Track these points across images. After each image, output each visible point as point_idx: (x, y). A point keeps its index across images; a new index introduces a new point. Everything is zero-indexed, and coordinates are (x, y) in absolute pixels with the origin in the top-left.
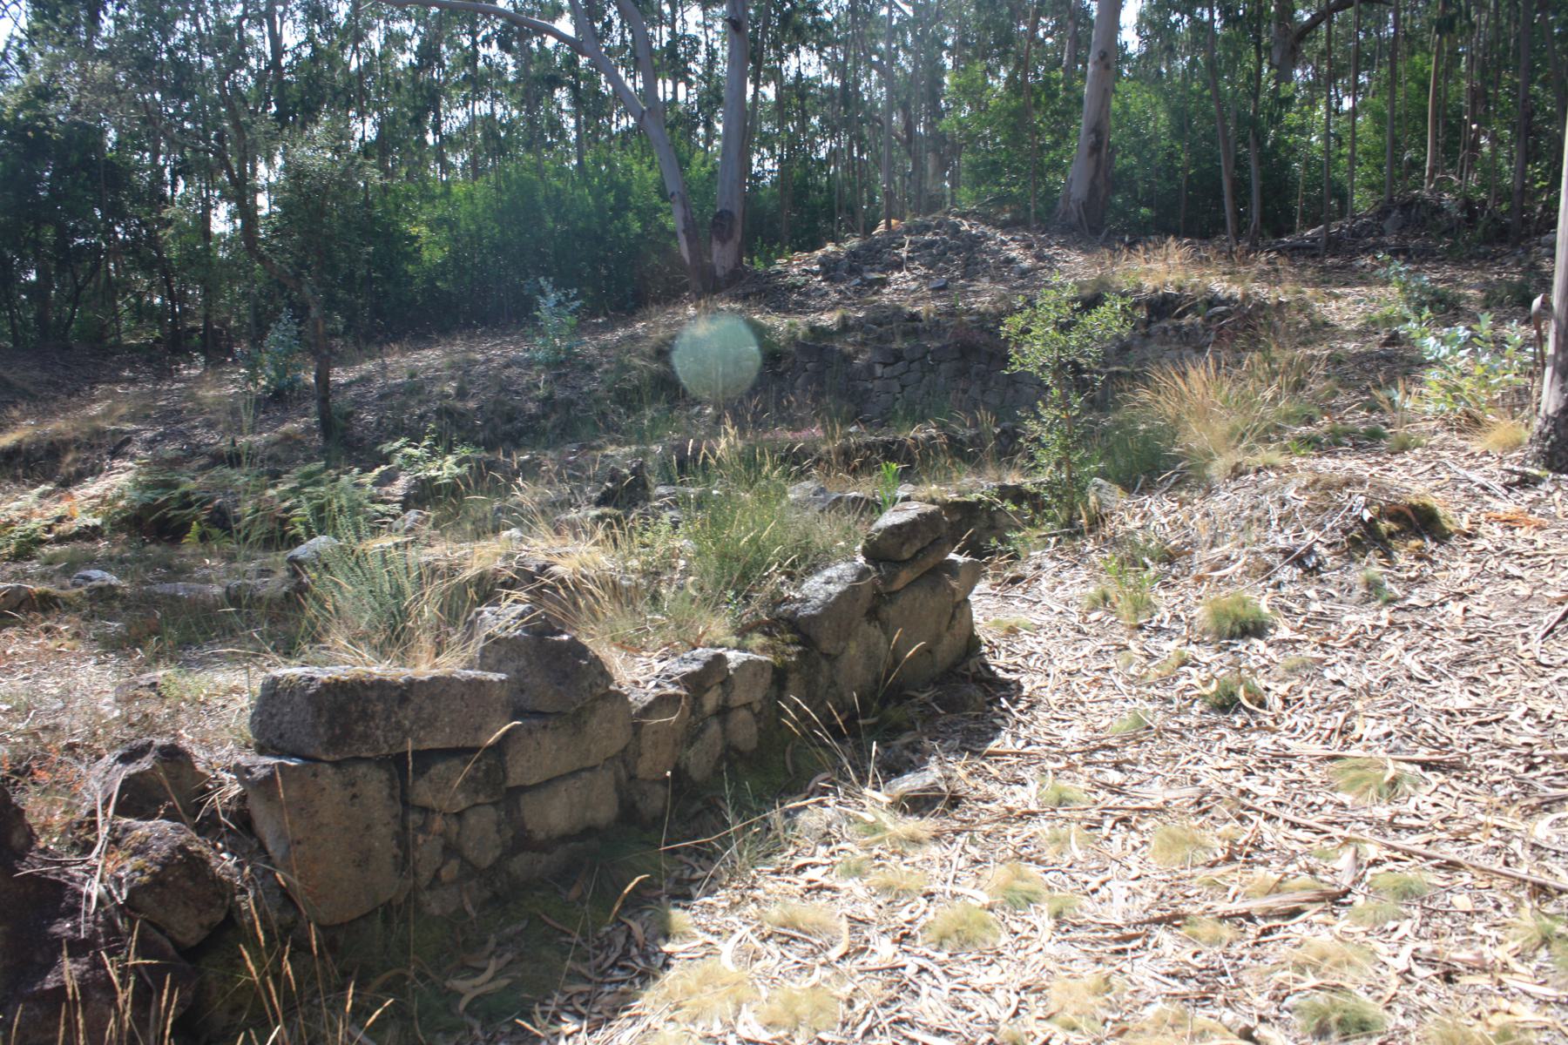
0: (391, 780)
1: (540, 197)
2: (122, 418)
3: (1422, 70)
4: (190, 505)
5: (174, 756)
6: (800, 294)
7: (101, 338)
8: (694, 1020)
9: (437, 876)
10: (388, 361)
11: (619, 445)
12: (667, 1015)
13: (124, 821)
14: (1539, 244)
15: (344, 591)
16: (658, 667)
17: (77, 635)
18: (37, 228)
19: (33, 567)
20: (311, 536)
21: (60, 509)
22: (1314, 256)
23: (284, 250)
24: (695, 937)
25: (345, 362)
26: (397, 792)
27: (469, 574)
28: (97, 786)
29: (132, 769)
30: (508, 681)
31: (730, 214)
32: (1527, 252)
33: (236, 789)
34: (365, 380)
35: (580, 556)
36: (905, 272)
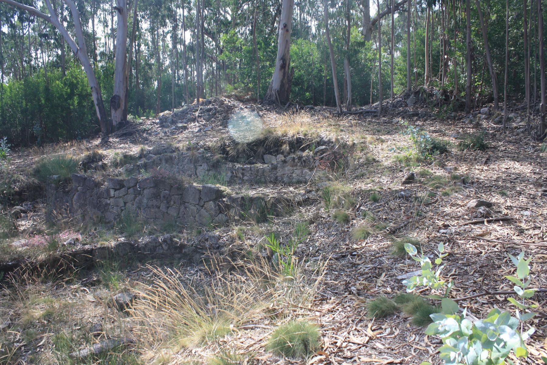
3: (421, 35)
6: (147, 134)
14: (480, 113)
22: (375, 116)
31: (119, 96)
32: (475, 116)
36: (196, 123)
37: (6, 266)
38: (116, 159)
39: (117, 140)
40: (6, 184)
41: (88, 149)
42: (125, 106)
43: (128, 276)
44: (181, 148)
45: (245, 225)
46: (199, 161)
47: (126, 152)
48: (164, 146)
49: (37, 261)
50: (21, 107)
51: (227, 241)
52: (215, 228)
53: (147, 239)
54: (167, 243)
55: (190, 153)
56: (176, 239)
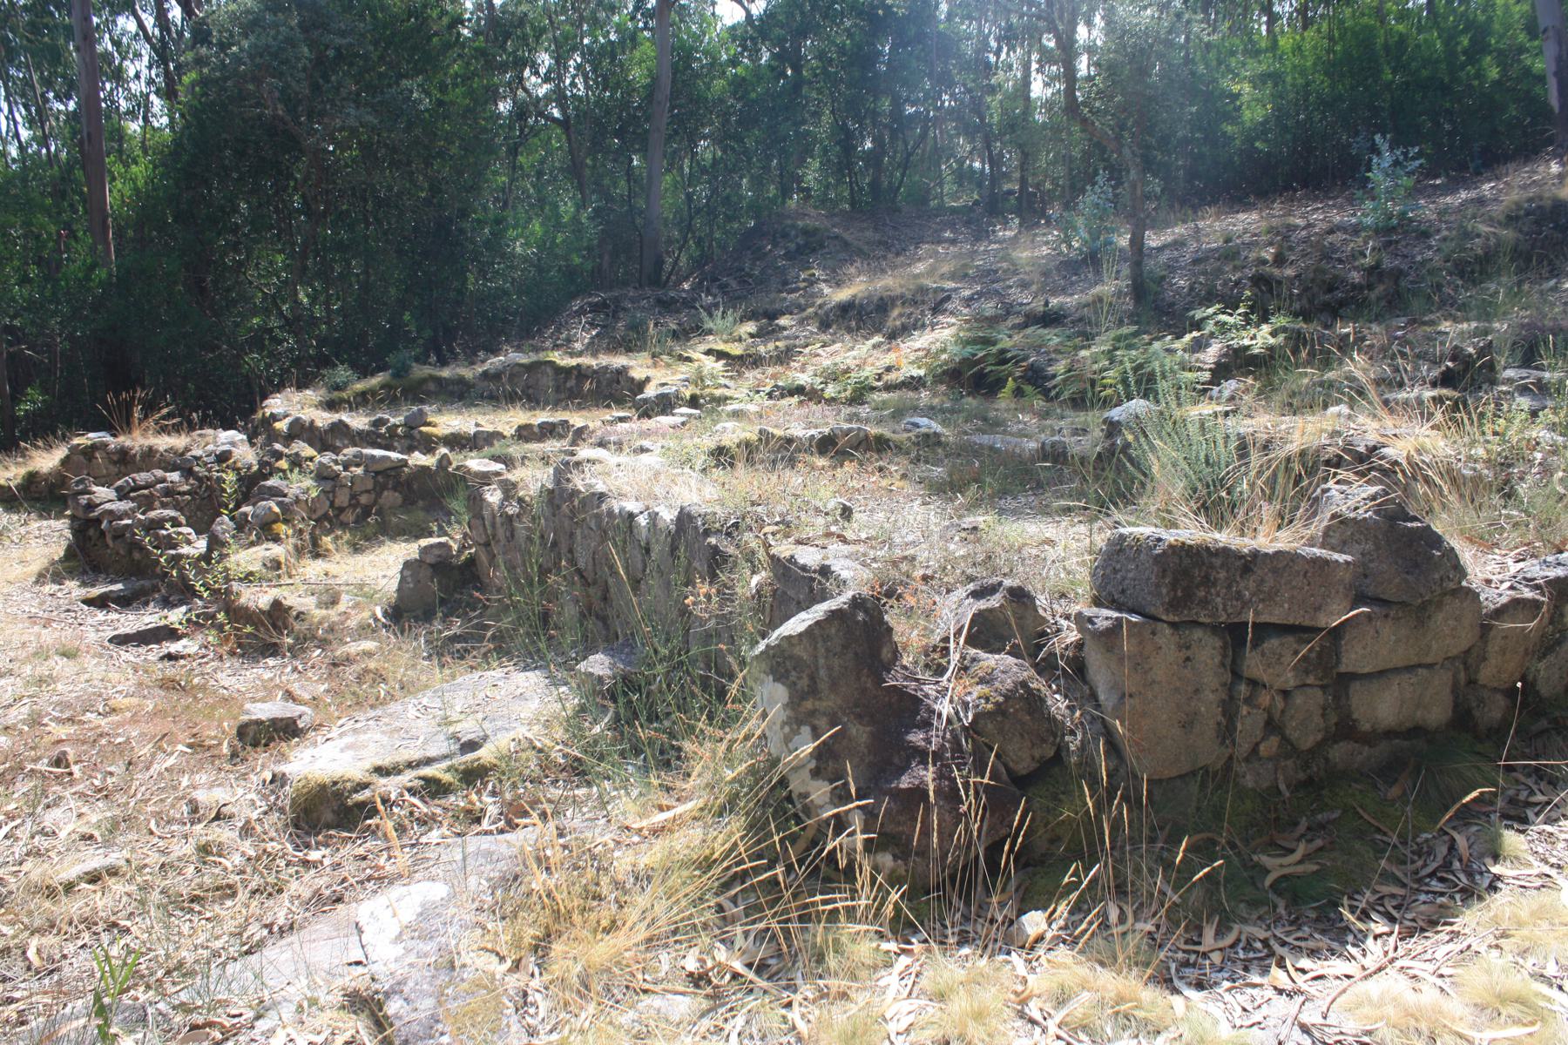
0: (1224, 648)
1: (1380, 41)
2: (942, 277)
4: (1005, 362)
5: (1020, 596)
7: (924, 201)
8: (1524, 953)
9: (1255, 750)
10: (1201, 224)
11: (1455, 320)
12: (1491, 940)
13: (972, 651)
15: (1161, 458)
16: (1514, 568)
17: (904, 476)
18: (876, 99)
19: (863, 411)
20: (1130, 398)
21: (890, 358)
23: (1106, 112)
24: (1530, 865)
25: (1159, 225)
26: (1228, 661)
27: (1293, 447)
28: (951, 616)
29: (983, 605)
30: (1354, 563)
33: (1072, 636)
34: (1178, 244)
35: (1415, 438)
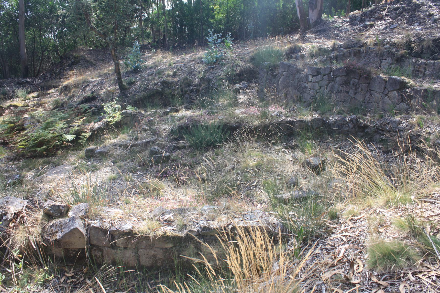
6: (338, 31)
36: (383, 21)
37: (231, 126)
38: (312, 51)
39: (313, 35)
40: (230, 68)
41: (290, 43)
42: (321, 7)
43: (319, 145)
44: (369, 43)
45: (425, 114)
46: (384, 55)
47: (321, 46)
48: (353, 42)
49: (252, 126)
50: (240, 9)
51: (407, 126)
52: (396, 114)
53: (336, 118)
54: (353, 122)
55: (376, 48)
56: (360, 120)
